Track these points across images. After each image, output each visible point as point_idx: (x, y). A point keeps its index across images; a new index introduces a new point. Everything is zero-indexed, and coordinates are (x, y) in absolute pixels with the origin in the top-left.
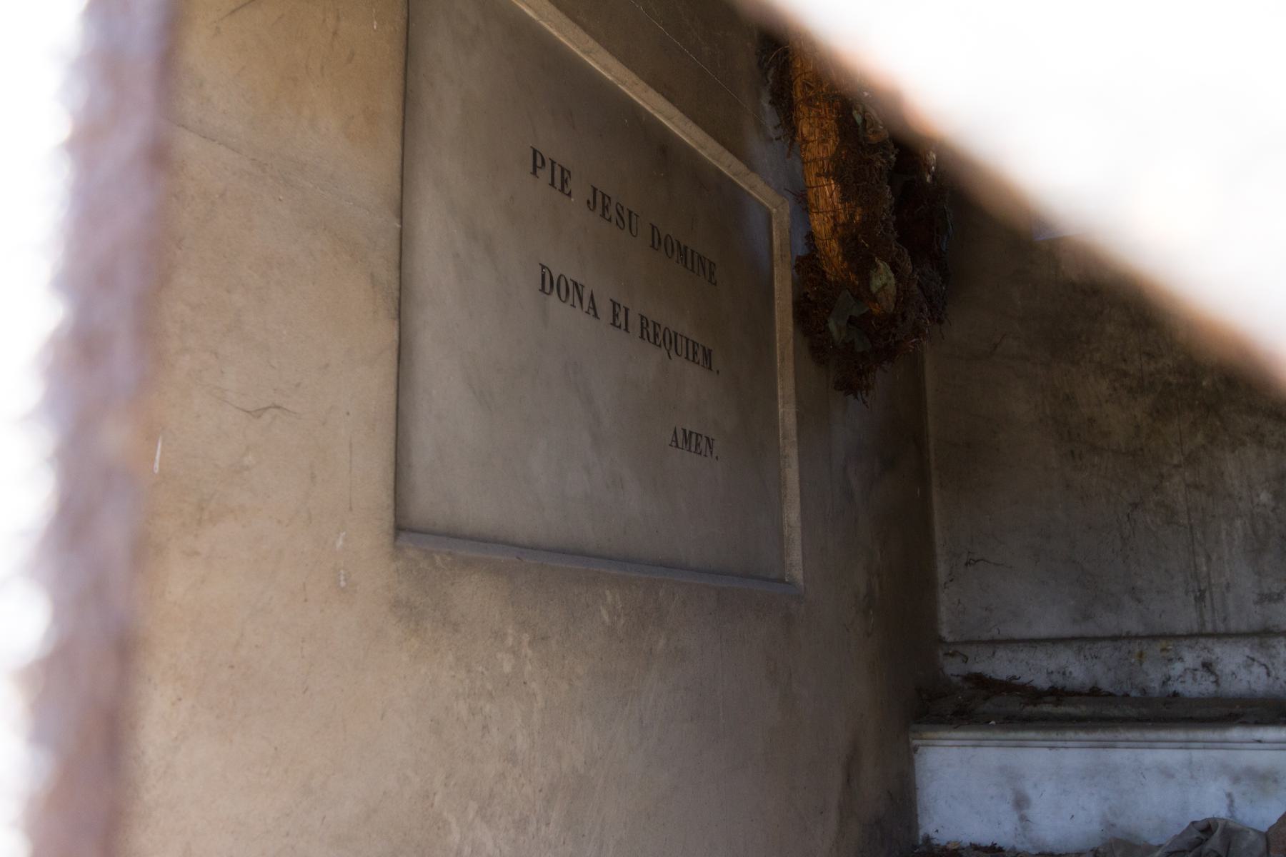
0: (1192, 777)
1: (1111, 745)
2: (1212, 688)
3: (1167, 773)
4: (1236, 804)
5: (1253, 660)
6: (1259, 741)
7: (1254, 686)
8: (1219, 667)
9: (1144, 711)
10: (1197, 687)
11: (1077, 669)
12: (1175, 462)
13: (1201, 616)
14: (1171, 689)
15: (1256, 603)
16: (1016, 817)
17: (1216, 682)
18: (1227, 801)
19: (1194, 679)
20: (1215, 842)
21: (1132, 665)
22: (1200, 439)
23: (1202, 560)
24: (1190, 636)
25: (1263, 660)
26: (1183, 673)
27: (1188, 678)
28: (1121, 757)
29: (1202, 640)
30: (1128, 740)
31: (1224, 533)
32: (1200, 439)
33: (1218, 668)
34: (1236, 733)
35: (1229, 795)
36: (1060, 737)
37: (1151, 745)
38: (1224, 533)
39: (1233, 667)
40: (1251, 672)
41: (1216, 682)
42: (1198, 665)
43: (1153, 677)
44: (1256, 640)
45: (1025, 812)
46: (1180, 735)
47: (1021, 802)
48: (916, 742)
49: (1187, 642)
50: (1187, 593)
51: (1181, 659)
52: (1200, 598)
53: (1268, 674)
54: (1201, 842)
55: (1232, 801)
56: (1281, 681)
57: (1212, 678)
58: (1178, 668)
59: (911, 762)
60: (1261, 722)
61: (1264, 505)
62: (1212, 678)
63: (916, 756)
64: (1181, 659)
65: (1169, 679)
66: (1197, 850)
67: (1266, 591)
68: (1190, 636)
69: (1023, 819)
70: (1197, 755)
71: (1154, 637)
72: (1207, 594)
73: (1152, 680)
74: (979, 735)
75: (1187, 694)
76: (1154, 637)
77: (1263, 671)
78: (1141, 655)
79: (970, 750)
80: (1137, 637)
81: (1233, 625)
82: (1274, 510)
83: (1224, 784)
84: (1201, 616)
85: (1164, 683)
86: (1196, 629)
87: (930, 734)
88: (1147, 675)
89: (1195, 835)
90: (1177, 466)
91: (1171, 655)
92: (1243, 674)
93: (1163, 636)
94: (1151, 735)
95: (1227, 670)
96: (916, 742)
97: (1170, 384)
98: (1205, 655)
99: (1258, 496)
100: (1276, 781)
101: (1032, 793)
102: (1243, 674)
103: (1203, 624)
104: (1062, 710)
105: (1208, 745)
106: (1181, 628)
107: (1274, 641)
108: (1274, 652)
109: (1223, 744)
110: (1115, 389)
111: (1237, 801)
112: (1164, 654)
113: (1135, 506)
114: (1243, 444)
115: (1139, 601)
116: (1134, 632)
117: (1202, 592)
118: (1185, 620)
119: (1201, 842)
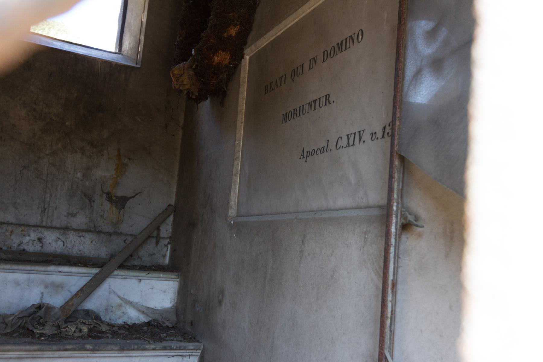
0: (28, 285)
3: (17, 283)
4: (44, 297)
5: (59, 239)
6: (60, 272)
8: (45, 240)
9: (10, 256)
10: (33, 248)
11: (396, 142)
12: (47, 153)
13: (42, 218)
14: (22, 247)
15: (65, 216)
17: (42, 247)
18: (41, 295)
19: (33, 244)
20: (42, 313)
21: (6, 235)
22: (59, 146)
23: (48, 196)
24: (35, 226)
25: (63, 239)
26: (29, 242)
27: (30, 244)
29: (40, 229)
30: (4, 269)
31: (60, 186)
32: (59, 146)
33: (44, 241)
34: (52, 268)
35: (42, 293)
37: (14, 271)
38: (60, 186)
39: (50, 241)
40: (57, 244)
41: (42, 247)
42: (36, 238)
43: (14, 242)
44: (62, 231)
46: (28, 267)
49: (34, 229)
50: (38, 208)
51: (29, 235)
52: (43, 211)
53: (64, 245)
55: (43, 296)
56: (68, 248)
57: (41, 245)
58: (27, 239)
60: (60, 264)
61: (78, 178)
62: (41, 245)
64: (29, 235)
65: (22, 243)
66: (32, 316)
67: (71, 212)
68: (35, 226)
70: (32, 276)
71: (19, 225)
72: (47, 210)
73: (14, 243)
75: (28, 250)
76: (19, 225)
77: (62, 243)
78: (12, 232)
80: (12, 224)
81: (55, 224)
82: (81, 181)
83: (41, 289)
84: (42, 218)
85: (19, 245)
86: (38, 223)
88: (12, 240)
89: (34, 309)
90: (47, 155)
91: (25, 233)
92: (54, 244)
93: (24, 225)
94: (15, 267)
95: (48, 242)
97: (53, 120)
98: (40, 235)
99: (77, 174)
100: (62, 288)
102: (54, 244)
103: (42, 222)
105: (38, 272)
106: (32, 221)
107: (69, 232)
108: (68, 236)
109: (46, 272)
110: (28, 115)
111: (45, 295)
112: (22, 232)
113: (25, 167)
114: (76, 152)
115: (16, 208)
116: (10, 222)
117: (45, 209)
118: (35, 219)
119: (35, 312)
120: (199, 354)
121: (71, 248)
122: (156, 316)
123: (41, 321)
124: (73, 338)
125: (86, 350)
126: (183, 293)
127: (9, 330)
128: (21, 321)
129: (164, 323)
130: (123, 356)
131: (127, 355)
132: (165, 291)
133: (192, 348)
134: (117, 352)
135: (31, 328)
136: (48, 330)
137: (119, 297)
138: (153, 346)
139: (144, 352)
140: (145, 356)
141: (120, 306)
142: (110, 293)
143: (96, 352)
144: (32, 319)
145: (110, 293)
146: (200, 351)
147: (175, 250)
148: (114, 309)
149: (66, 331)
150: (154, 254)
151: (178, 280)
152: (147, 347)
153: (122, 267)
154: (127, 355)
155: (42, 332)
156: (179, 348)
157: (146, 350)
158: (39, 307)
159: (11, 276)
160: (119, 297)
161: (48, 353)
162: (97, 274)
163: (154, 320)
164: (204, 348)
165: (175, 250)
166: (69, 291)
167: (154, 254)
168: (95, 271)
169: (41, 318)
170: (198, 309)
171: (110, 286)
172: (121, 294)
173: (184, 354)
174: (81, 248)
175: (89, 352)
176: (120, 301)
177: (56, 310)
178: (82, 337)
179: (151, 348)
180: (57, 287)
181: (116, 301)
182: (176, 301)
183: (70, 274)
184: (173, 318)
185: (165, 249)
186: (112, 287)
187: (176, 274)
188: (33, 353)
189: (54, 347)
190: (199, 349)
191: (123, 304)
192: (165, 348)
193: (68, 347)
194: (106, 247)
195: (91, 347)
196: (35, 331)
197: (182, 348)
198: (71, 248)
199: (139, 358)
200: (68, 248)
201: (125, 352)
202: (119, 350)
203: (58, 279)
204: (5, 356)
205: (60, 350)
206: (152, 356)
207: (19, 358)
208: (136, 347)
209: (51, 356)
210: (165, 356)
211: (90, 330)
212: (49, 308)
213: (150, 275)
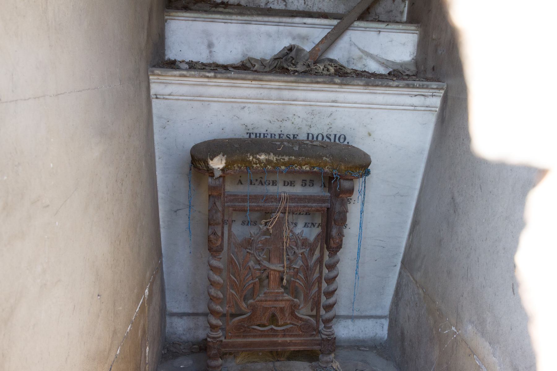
1: (248, 23)
2: (284, 8)
3: (269, 35)
6: (305, 23)
7: (299, 8)
14: (269, 7)
16: (208, 51)
17: (286, 5)
20: (293, 54)
28: (252, 28)
36: (230, 18)
37: (265, 23)
40: (299, 2)
41: (286, 5)
45: (212, 49)
46: (277, 19)
47: (210, 45)
48: (166, 17)
53: (305, 3)
54: (287, 54)
56: (309, 7)
57: (284, 3)
59: (164, 26)
62: (284, 3)
63: (166, 24)
69: (210, 52)
70: (281, 28)
74: (196, 15)
79: (190, 22)
85: (266, 4)
87: (174, 14)
89: (286, 51)
96: (166, 17)
100: (307, 39)
101: (215, 41)
104: (227, 10)
105: (286, 24)
109: (292, 24)
119: (287, 54)
120: (442, 95)
121: (311, 6)
122: (395, 68)
123: (293, 62)
124: (322, 75)
125: (335, 84)
126: (423, 45)
127: (267, 69)
128: (276, 62)
129: (405, 72)
130: (368, 93)
131: (371, 91)
132: (404, 44)
133: (435, 87)
134: (362, 88)
135: (285, 66)
136: (300, 68)
137: (359, 49)
138: (396, 83)
139: (387, 89)
140: (388, 94)
141: (361, 58)
142: (351, 45)
143: (344, 87)
144: (286, 60)
145: (351, 45)
146: (443, 92)
147: (413, 3)
148: (355, 61)
149: (316, 69)
150: (391, 11)
151: (417, 32)
152: (391, 83)
153: (362, 17)
154: (371, 91)
155: (295, 69)
156: (422, 87)
157: (390, 86)
158: (290, 49)
159: (264, 28)
160: (359, 49)
161: (302, 85)
162: (336, 26)
163: (394, 70)
164: (447, 88)
165: (413, 3)
166: (313, 43)
167: (391, 11)
168: (335, 22)
169: (293, 59)
170: (440, 52)
171: (350, 38)
172: (361, 46)
173: (426, 94)
174: (321, 6)
175: (337, 86)
176: (361, 54)
177: (305, 53)
178: (329, 75)
179: (395, 85)
180: (305, 38)
181: (356, 53)
182: (415, 55)
183: (313, 26)
184: (413, 68)
185: (403, 5)
186: (353, 40)
187: (416, 25)
188: (290, 84)
189: (308, 80)
190: (442, 89)
191: (364, 57)
192: (408, 86)
193: (319, 80)
194: (344, 5)
195: (339, 81)
196: (289, 68)
197: (425, 86)
198: (311, 6)
199: (383, 95)
200: (309, 7)
201: (370, 88)
202: (364, 85)
203: (303, 31)
204: (268, 86)
205: (312, 83)
206: (395, 94)
207: (279, 89)
208: (380, 83)
209: (305, 88)
210: (408, 94)
211: (336, 71)
212: (300, 50)
213: (389, 27)
